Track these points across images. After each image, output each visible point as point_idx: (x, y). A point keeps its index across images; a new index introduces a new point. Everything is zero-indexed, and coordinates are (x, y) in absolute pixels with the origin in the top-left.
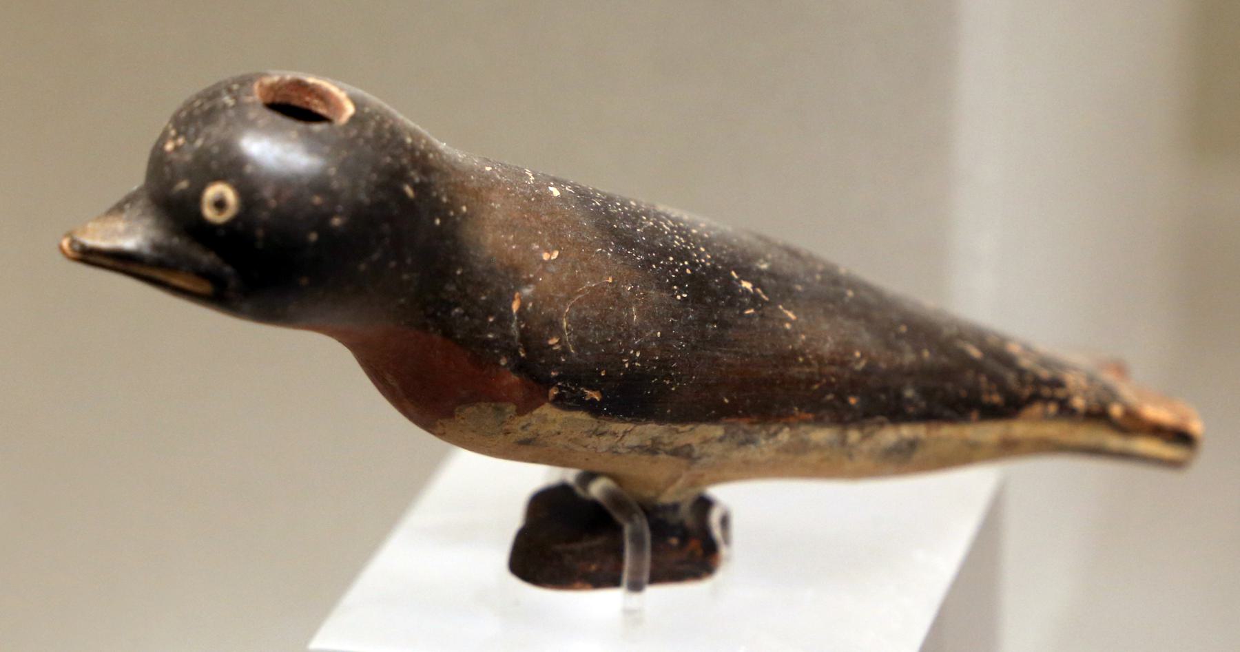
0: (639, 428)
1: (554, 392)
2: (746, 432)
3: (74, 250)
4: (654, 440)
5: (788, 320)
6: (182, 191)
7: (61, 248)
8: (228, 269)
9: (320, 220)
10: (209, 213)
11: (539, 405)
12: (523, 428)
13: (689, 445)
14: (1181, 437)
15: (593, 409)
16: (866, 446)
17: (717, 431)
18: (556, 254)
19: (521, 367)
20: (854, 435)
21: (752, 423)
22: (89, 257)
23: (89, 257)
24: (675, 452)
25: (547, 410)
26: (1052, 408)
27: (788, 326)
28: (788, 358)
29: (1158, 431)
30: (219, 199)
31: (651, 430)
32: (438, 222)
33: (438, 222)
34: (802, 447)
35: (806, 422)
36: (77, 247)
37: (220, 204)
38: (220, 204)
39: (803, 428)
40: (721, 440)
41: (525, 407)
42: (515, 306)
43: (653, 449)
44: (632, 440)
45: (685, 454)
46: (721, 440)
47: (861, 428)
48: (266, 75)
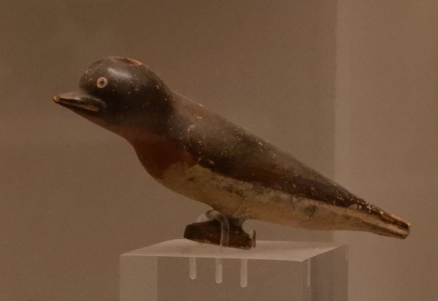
0: (226, 179)
1: (200, 159)
2: (261, 189)
3: (57, 100)
4: (231, 185)
5: (274, 156)
6: (91, 81)
7: (54, 100)
8: (103, 103)
9: (132, 88)
10: (99, 86)
11: (195, 164)
12: (190, 173)
13: (242, 190)
14: (404, 226)
15: (211, 167)
16: (299, 205)
17: (250, 186)
18: (201, 118)
19: (190, 150)
20: (295, 199)
21: (262, 186)
22: (62, 102)
23: (62, 102)
24: (237, 193)
25: (197, 166)
26: (360, 207)
27: (273, 157)
28: (274, 166)
29: (395, 222)
30: (102, 82)
31: (229, 181)
32: (166, 100)
33: (166, 100)
34: (277, 200)
35: (280, 190)
36: (58, 99)
37: (102, 83)
38: (102, 83)
39: (278, 192)
40: (252, 190)
41: (191, 165)
42: (189, 130)
43: (230, 189)
44: (223, 184)
45: (239, 193)
46: (252, 190)
47: (297, 198)
48: (118, 59)
